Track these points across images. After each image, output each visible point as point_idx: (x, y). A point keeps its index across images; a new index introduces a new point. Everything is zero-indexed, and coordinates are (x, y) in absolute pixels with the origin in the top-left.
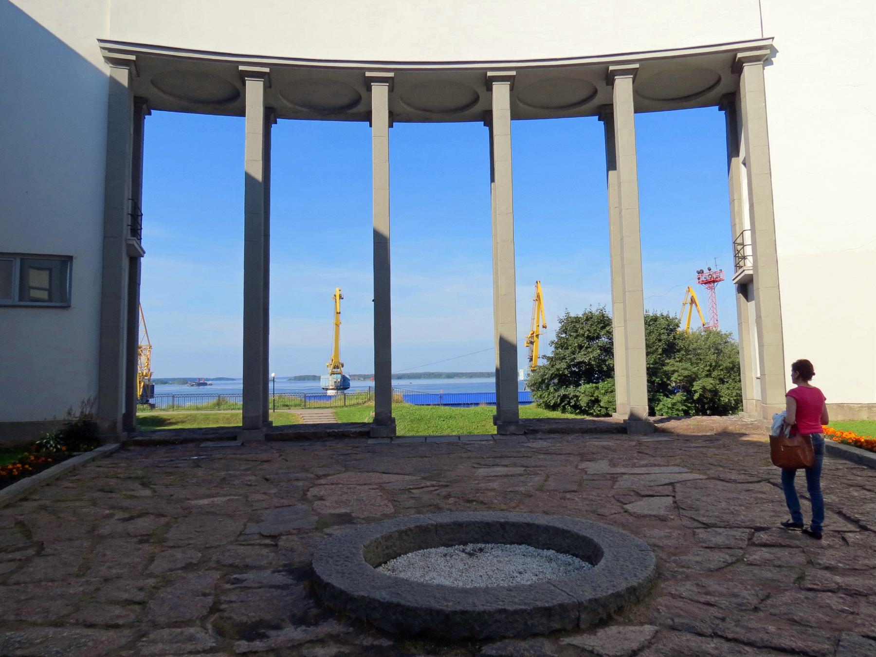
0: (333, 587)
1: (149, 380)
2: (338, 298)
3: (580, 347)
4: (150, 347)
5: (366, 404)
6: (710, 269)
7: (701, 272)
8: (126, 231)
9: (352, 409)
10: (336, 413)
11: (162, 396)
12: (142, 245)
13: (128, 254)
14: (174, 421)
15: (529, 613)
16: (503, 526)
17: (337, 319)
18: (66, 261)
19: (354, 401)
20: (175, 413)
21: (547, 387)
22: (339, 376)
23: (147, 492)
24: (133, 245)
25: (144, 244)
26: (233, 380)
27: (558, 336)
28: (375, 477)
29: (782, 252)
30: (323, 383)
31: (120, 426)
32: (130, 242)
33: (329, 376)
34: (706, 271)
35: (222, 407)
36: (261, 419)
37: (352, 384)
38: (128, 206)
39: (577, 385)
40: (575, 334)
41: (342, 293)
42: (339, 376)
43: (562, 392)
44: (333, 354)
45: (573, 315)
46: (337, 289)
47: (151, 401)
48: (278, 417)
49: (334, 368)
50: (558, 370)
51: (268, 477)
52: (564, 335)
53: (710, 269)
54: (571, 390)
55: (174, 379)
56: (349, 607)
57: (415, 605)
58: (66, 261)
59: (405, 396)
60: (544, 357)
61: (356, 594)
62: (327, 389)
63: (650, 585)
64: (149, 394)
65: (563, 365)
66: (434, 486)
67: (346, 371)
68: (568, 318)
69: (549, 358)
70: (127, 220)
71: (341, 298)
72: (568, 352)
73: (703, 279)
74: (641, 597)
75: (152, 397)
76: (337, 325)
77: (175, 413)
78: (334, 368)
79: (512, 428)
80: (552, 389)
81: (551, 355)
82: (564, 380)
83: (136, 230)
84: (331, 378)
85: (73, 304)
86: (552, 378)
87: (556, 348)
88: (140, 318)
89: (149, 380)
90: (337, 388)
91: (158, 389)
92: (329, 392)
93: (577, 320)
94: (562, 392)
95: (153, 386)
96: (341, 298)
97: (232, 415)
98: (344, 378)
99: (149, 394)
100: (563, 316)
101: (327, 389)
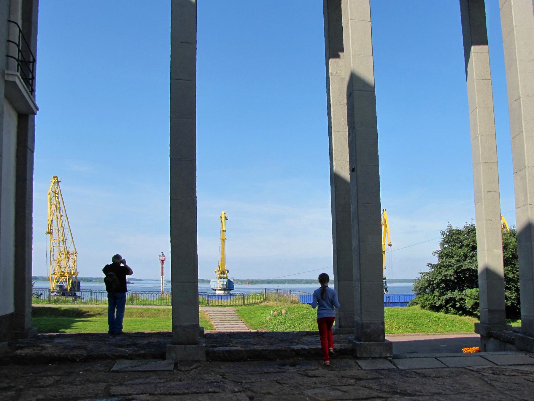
1: (76, 278)
2: (223, 219)
3: (465, 256)
4: (76, 252)
5: (263, 304)
9: (251, 307)
10: (238, 311)
11: (86, 290)
12: (37, 102)
14: (92, 313)
17: (223, 235)
19: (252, 301)
20: (94, 306)
21: (433, 291)
22: (226, 280)
24: (14, 83)
25: (38, 101)
26: (141, 280)
30: (213, 285)
32: (11, 79)
33: (217, 280)
35: (135, 302)
37: (235, 286)
39: (461, 290)
40: (458, 245)
41: (227, 215)
42: (226, 280)
43: (449, 295)
44: (220, 262)
46: (223, 212)
47: (78, 294)
48: (217, 319)
49: (221, 273)
50: (445, 276)
52: (446, 246)
54: (456, 294)
55: (97, 278)
59: (302, 297)
60: (429, 265)
62: (216, 290)
64: (76, 289)
65: (450, 272)
67: (231, 276)
69: (434, 266)
71: (226, 219)
72: (453, 261)
75: (79, 290)
76: (223, 241)
77: (94, 306)
78: (221, 273)
80: (436, 293)
82: (449, 285)
84: (218, 281)
86: (439, 284)
89: (76, 278)
90: (224, 289)
91: (82, 285)
92: (217, 292)
93: (459, 232)
94: (449, 295)
95: (79, 283)
96: (226, 219)
97: (145, 310)
98: (229, 282)
99: (76, 289)
100: (445, 229)
101: (216, 290)
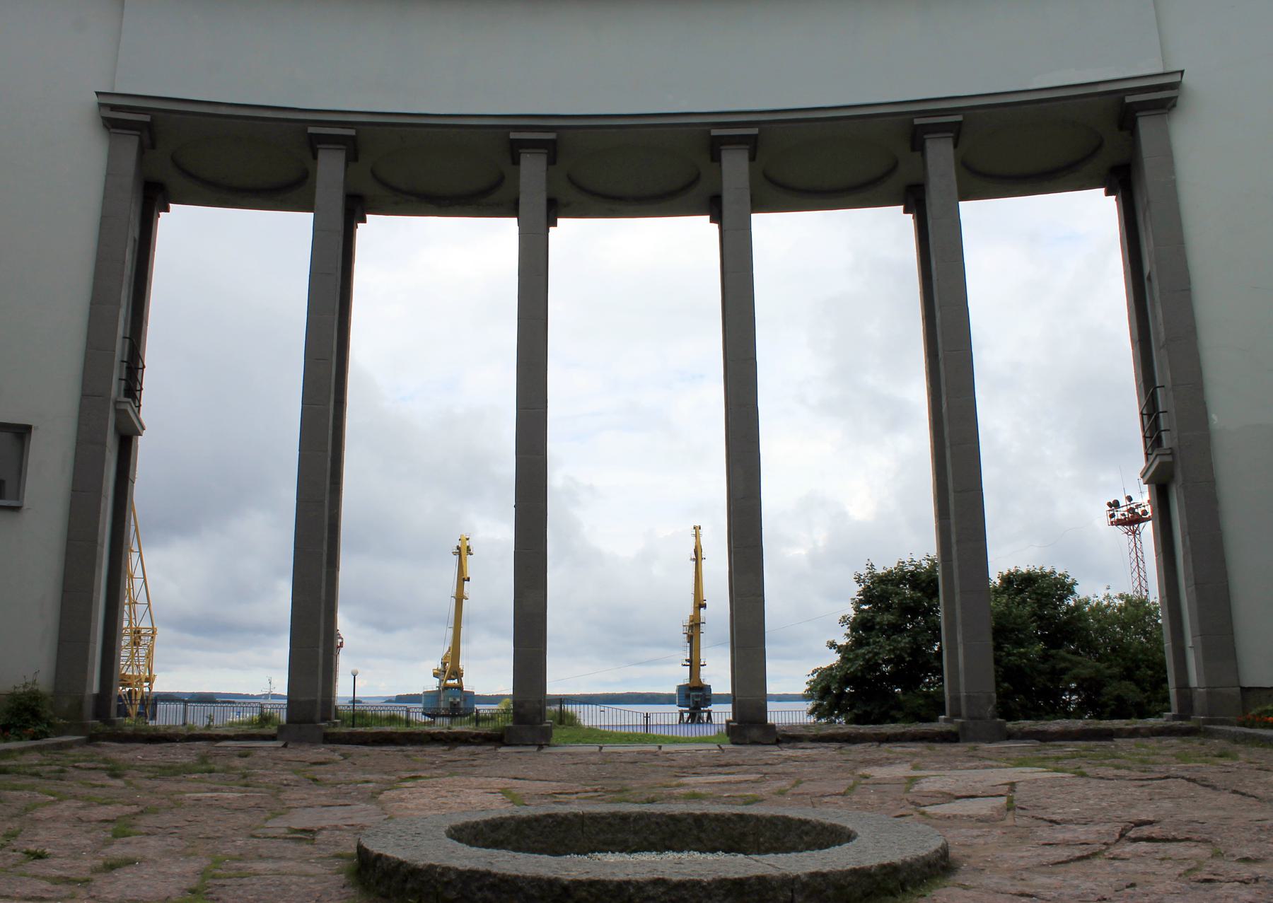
0: (387, 858)
6: (1129, 499)
7: (1115, 505)
8: (116, 388)
12: (142, 416)
13: (116, 428)
15: (703, 887)
16: (699, 820)
18: (22, 433)
23: (119, 783)
24: (126, 411)
27: (857, 609)
28: (498, 783)
29: (1215, 419)
31: (88, 708)
32: (122, 407)
34: (1123, 502)
36: (319, 707)
38: (120, 349)
45: (880, 571)
51: (318, 777)
53: (1129, 499)
56: (409, 886)
57: (515, 873)
58: (22, 433)
61: (421, 863)
63: (926, 870)
66: (596, 791)
68: (873, 576)
69: (840, 649)
70: (118, 372)
73: (1118, 516)
74: (855, 798)
79: (755, 733)
81: (843, 641)
83: (132, 388)
85: (28, 500)
87: (853, 629)
88: (133, 529)
